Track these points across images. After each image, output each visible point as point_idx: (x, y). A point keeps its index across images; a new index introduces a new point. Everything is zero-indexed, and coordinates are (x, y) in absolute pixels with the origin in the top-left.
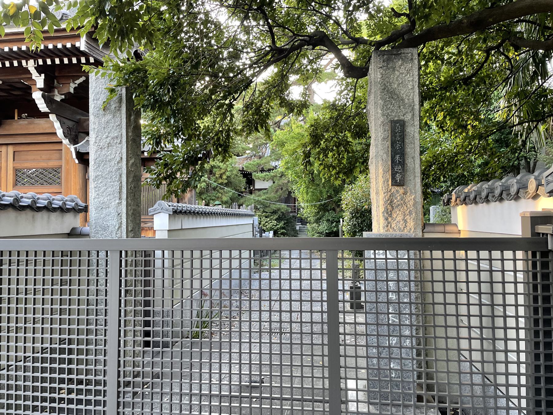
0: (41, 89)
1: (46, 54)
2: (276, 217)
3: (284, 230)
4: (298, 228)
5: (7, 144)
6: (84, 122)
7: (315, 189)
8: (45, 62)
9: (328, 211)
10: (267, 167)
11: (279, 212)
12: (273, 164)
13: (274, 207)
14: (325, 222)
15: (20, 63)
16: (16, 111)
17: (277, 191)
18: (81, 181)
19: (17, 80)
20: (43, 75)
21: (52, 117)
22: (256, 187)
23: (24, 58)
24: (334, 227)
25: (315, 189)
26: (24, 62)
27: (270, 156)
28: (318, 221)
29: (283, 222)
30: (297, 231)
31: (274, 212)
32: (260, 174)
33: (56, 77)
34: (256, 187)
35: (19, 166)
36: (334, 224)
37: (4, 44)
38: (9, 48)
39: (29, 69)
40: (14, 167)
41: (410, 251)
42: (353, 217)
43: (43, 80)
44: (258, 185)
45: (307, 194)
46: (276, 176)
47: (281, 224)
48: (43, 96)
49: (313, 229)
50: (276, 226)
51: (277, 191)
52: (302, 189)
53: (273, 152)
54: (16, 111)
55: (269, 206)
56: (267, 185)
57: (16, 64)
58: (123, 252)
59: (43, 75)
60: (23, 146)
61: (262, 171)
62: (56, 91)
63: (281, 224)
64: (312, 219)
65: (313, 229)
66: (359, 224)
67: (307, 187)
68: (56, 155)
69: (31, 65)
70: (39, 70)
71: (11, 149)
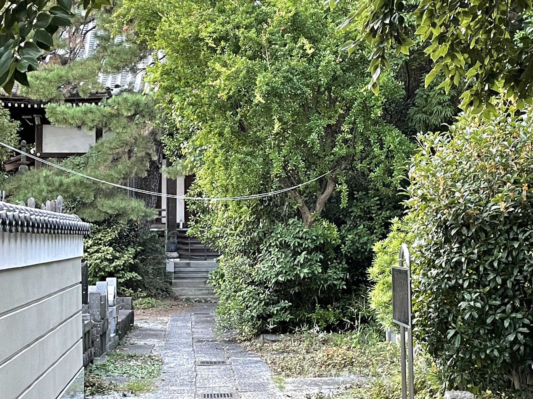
2: (112, 235)
3: (134, 274)
4: (170, 268)
7: (251, 154)
9: (284, 220)
10: (86, 87)
11: (122, 222)
12: (106, 80)
13: (108, 206)
14: (274, 251)
17: (115, 160)
22: (47, 149)
24: (302, 266)
25: (251, 154)
27: (96, 58)
28: (252, 250)
29: (132, 250)
30: (167, 275)
31: (108, 222)
32: (63, 108)
34: (47, 149)
36: (301, 258)
41: (81, 285)
42: (448, 240)
44: (52, 141)
45: (227, 166)
46: (118, 115)
47: (127, 256)
49: (236, 271)
50: (111, 261)
51: (115, 160)
52: (210, 152)
53: (105, 49)
55: (92, 205)
56: (82, 142)
61: (74, 99)
63: (127, 256)
64: (234, 243)
65: (236, 271)
66: (470, 261)
67: (227, 148)
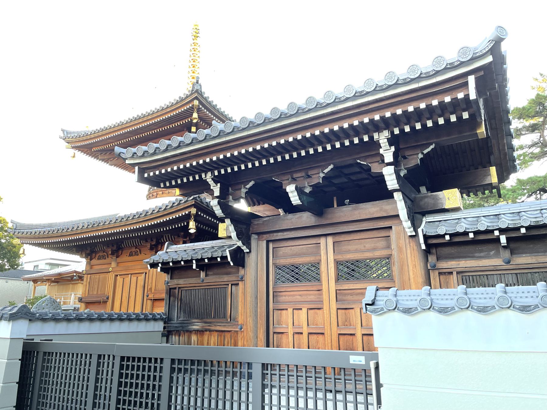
0: (217, 197)
1: (227, 164)
5: (326, 235)
6: (421, 200)
8: (219, 172)
15: (200, 176)
16: (335, 198)
18: (423, 273)
19: (351, 162)
20: (219, 184)
21: (398, 196)
23: (203, 171)
26: (203, 176)
33: (230, 185)
35: (340, 258)
37: (333, 124)
38: (224, 156)
39: (208, 180)
40: (335, 260)
43: (392, 153)
48: (219, 203)
54: (335, 198)
57: (366, 138)
58: (111, 356)
59: (219, 184)
60: (343, 236)
62: (231, 197)
68: (382, 243)
69: (208, 177)
70: (216, 180)
71: (330, 240)
